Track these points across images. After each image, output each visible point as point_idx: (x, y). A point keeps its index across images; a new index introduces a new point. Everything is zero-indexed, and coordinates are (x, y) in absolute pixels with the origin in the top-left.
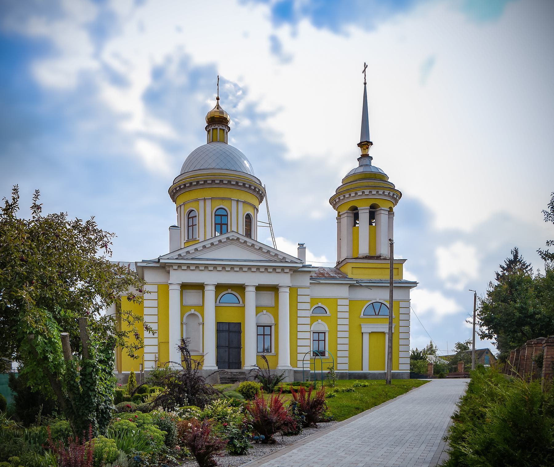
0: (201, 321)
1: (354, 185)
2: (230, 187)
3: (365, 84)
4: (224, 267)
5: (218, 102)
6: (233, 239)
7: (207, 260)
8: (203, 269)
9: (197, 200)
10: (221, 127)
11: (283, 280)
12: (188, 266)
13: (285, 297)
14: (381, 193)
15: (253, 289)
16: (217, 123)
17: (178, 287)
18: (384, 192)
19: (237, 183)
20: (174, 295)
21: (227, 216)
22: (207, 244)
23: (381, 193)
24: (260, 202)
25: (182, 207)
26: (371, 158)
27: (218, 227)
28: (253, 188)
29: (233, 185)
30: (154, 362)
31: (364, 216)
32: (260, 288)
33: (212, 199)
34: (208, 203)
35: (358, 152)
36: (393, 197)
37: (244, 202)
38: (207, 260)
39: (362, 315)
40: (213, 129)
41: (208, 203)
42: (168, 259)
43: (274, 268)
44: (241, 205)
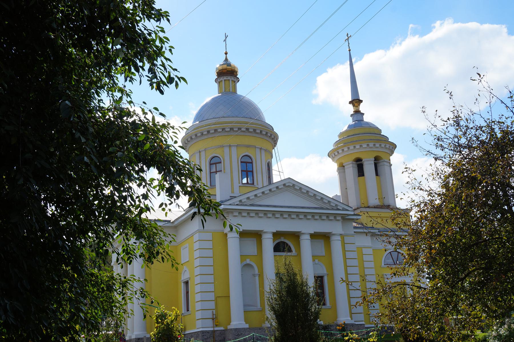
0: (257, 272)
1: (356, 138)
2: (255, 135)
3: (350, 50)
6: (289, 186)
9: (222, 146)
11: (335, 228)
13: (336, 244)
14: (383, 146)
15: (308, 237)
16: (227, 74)
18: (385, 146)
19: (261, 132)
20: (233, 241)
21: (252, 163)
23: (383, 146)
25: (203, 154)
26: (363, 114)
28: (269, 135)
29: (257, 133)
30: (211, 320)
31: (369, 168)
32: (314, 236)
34: (234, 149)
35: (351, 109)
36: (389, 149)
39: (383, 265)
40: (225, 80)
41: (234, 149)
42: (230, 205)
43: (328, 215)
44: (263, 152)
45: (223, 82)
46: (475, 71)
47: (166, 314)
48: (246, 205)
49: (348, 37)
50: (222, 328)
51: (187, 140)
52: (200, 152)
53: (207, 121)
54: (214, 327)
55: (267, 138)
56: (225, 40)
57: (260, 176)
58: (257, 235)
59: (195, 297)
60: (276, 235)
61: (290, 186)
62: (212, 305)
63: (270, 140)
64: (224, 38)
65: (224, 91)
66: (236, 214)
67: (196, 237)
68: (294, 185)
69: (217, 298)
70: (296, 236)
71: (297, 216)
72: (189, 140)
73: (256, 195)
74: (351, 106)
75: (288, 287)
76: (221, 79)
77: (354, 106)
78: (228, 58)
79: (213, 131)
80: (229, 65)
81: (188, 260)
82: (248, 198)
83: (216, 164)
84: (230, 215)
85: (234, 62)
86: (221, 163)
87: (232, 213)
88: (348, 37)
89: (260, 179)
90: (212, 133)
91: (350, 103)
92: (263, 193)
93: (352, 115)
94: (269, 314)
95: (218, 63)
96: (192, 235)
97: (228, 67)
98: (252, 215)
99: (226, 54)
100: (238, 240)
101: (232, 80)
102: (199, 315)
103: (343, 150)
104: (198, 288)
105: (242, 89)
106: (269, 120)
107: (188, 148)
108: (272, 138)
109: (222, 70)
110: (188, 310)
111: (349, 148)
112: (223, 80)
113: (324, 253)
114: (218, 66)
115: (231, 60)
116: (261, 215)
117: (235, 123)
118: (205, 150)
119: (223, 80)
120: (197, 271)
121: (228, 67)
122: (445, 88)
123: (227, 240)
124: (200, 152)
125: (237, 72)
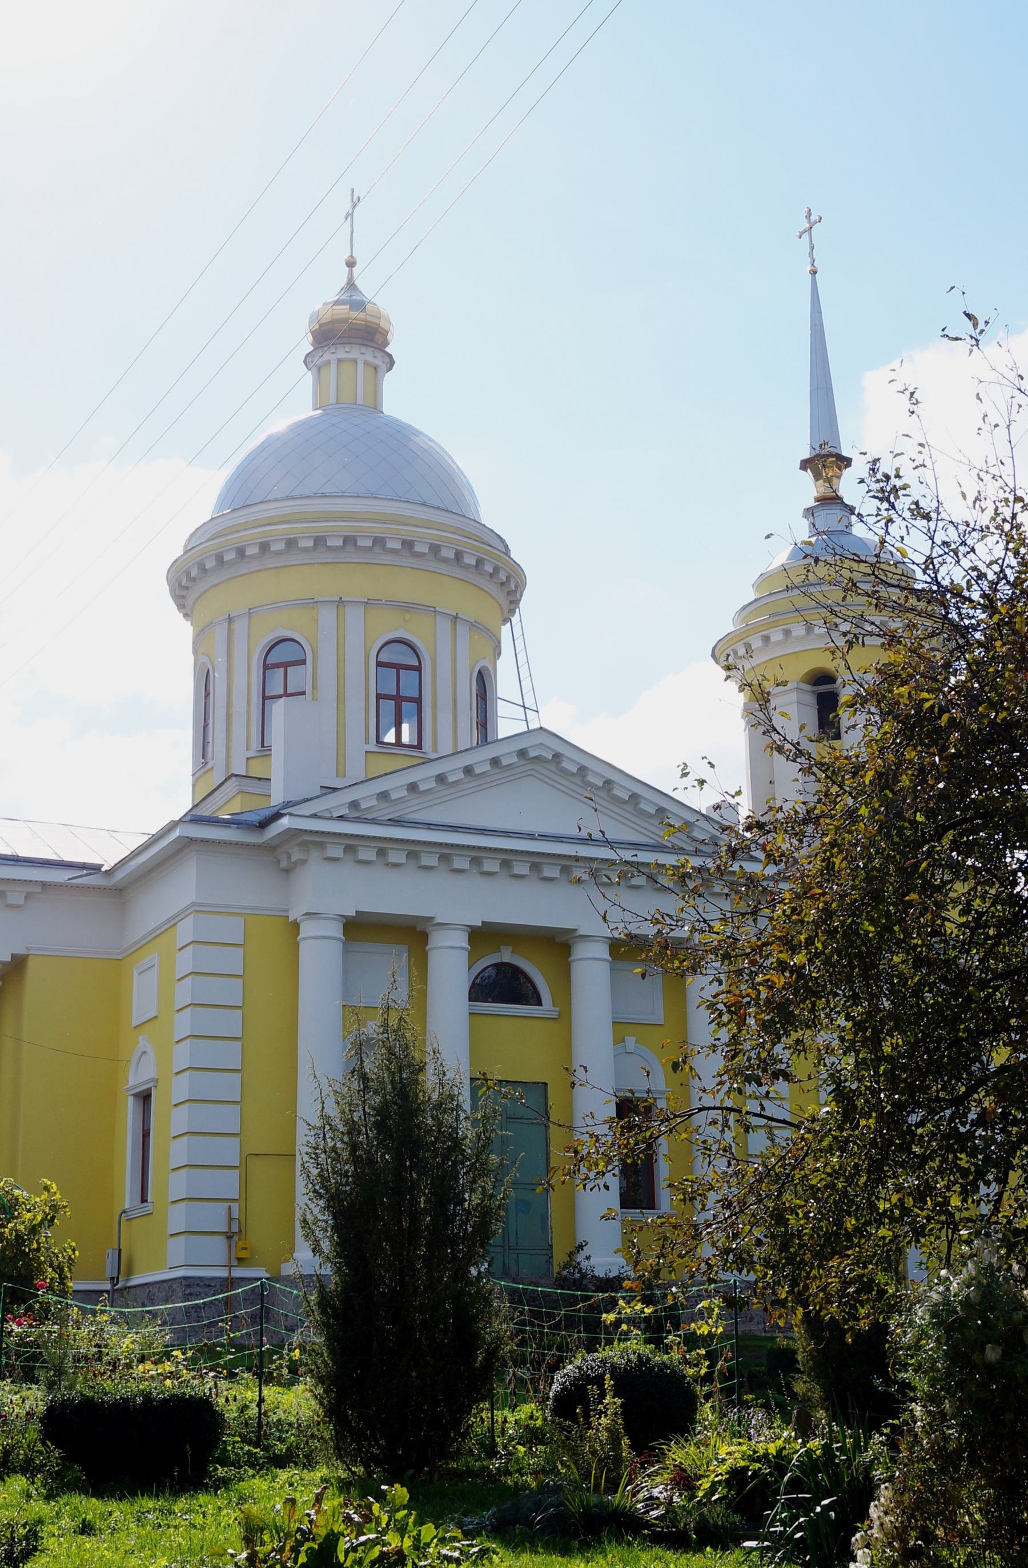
3: (814, 272)
4: (507, 859)
5: (351, 274)
7: (430, 826)
8: (21, 901)
10: (369, 357)
12: (383, 847)
15: (602, 951)
16: (351, 338)
17: (336, 930)
20: (320, 956)
21: (418, 669)
22: (453, 768)
24: (507, 620)
25: (240, 627)
27: (389, 706)
28: (489, 568)
29: (445, 561)
30: (220, 1242)
33: (368, 604)
34: (354, 617)
37: (473, 625)
38: (430, 826)
40: (339, 361)
41: (354, 617)
42: (315, 816)
44: (462, 629)
45: (333, 366)
46: (957, 305)
47: (15, 1202)
48: (374, 821)
49: (812, 222)
50: (261, 1273)
51: (188, 573)
52: (230, 620)
53: (264, 507)
54: (230, 1267)
55: (482, 582)
56: (350, 215)
57: (445, 718)
58: (412, 934)
59: (171, 1151)
60: (482, 937)
61: (549, 760)
62: (229, 1185)
63: (494, 589)
64: (348, 207)
65: (332, 399)
66: (335, 851)
67: (185, 931)
68: (557, 756)
69: (248, 1158)
70: (558, 944)
71: (565, 870)
72: (194, 573)
73: (413, 787)
74: (808, 476)
75: (382, 1111)
76: (327, 356)
77: (817, 476)
78: (358, 283)
79: (281, 546)
80: (360, 305)
81: (154, 1014)
82: (384, 796)
83: (286, 665)
84: (314, 856)
85: (386, 299)
86: (303, 662)
87: (321, 846)
88: (812, 222)
89: (448, 726)
90: (278, 553)
91: (805, 465)
92: (441, 778)
93: (810, 512)
94: (307, 1205)
95: (320, 294)
96: (172, 924)
97: (354, 314)
98: (394, 857)
99: (351, 264)
100: (335, 949)
101: (366, 363)
102: (178, 1218)
103: (766, 639)
104: (180, 1120)
105: (400, 398)
106: (494, 512)
107: (189, 603)
108: (495, 577)
109: (333, 322)
110: (144, 1200)
111: (787, 633)
112: (333, 358)
113: (659, 1017)
114: (318, 306)
115: (367, 288)
116: (461, 863)
117: (374, 521)
118: (250, 613)
119: (333, 358)
120: (182, 1056)
121: (354, 314)
122: (893, 376)
123: (296, 946)
124: (230, 620)
125: (385, 333)
